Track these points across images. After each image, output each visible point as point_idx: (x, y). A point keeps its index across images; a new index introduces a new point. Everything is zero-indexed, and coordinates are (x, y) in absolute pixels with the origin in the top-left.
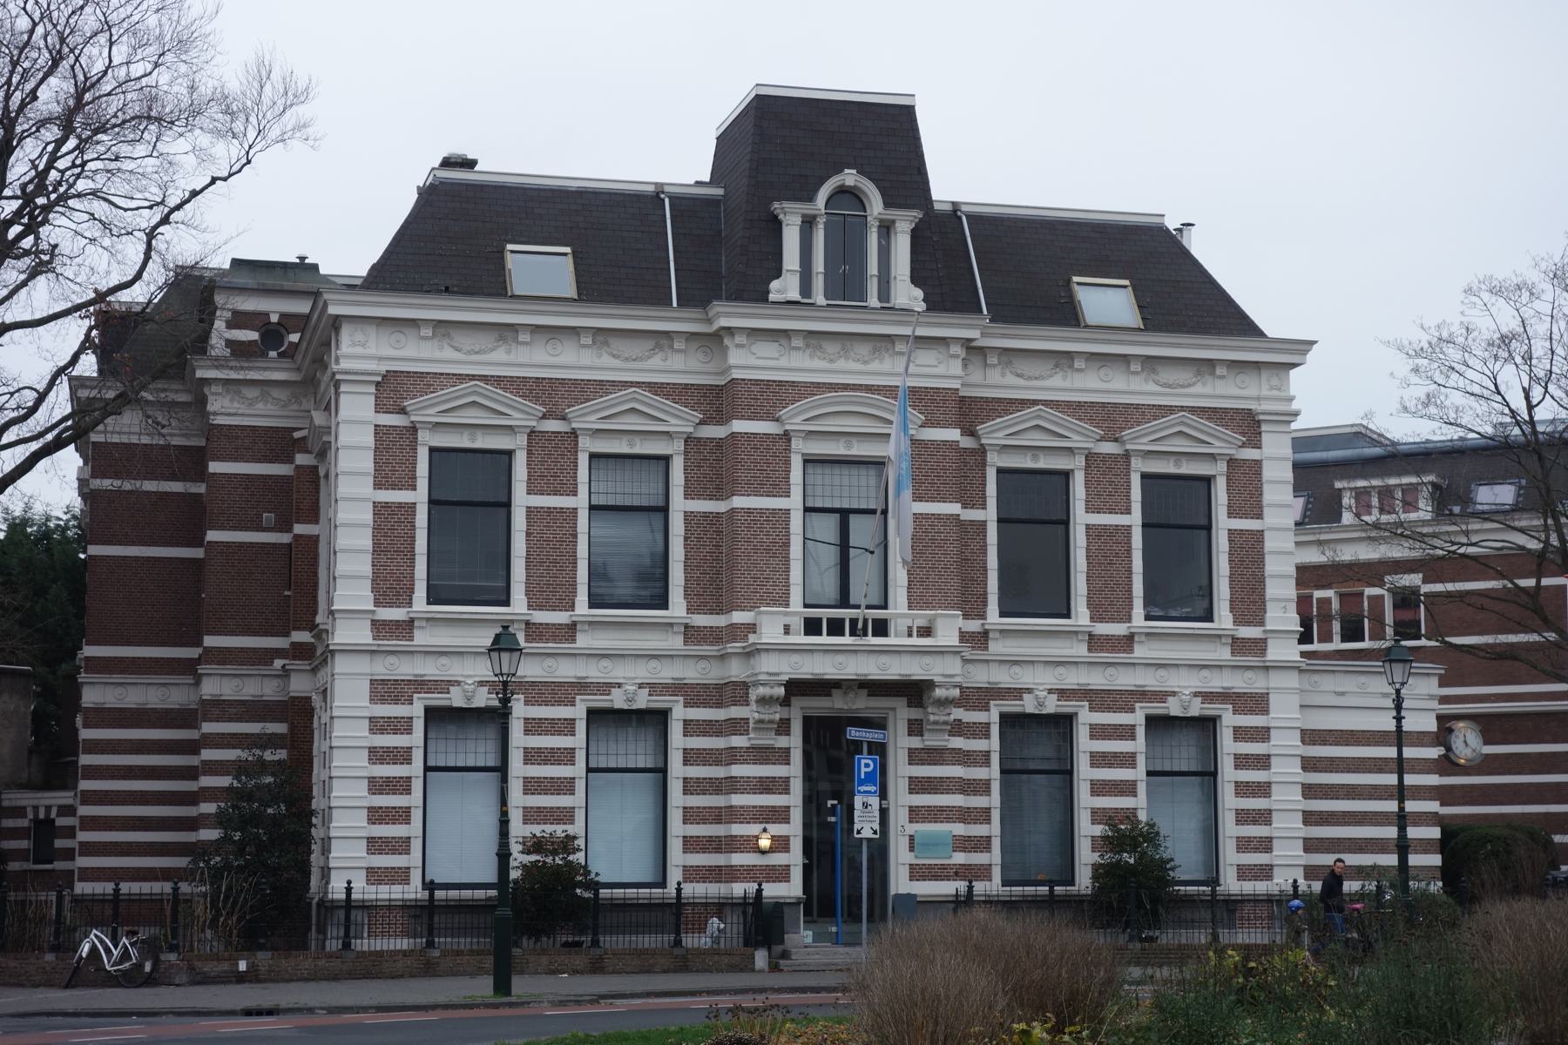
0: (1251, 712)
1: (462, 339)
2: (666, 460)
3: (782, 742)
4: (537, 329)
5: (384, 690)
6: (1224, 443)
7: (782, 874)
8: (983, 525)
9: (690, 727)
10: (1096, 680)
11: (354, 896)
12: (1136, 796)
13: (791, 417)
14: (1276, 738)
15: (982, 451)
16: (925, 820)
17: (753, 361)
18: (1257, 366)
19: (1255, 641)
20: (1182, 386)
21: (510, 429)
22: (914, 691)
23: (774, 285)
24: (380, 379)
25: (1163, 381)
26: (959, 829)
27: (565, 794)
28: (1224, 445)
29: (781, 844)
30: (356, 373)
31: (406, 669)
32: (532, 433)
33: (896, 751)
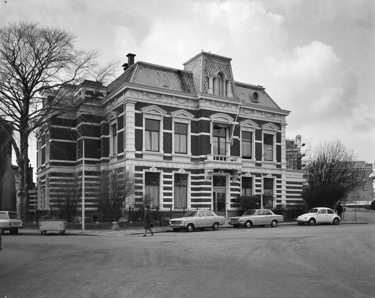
1: (151, 96)
6: (276, 129)
10: (165, 165)
11: (172, 210)
21: (188, 119)
24: (136, 103)
31: (141, 164)
32: (256, 130)
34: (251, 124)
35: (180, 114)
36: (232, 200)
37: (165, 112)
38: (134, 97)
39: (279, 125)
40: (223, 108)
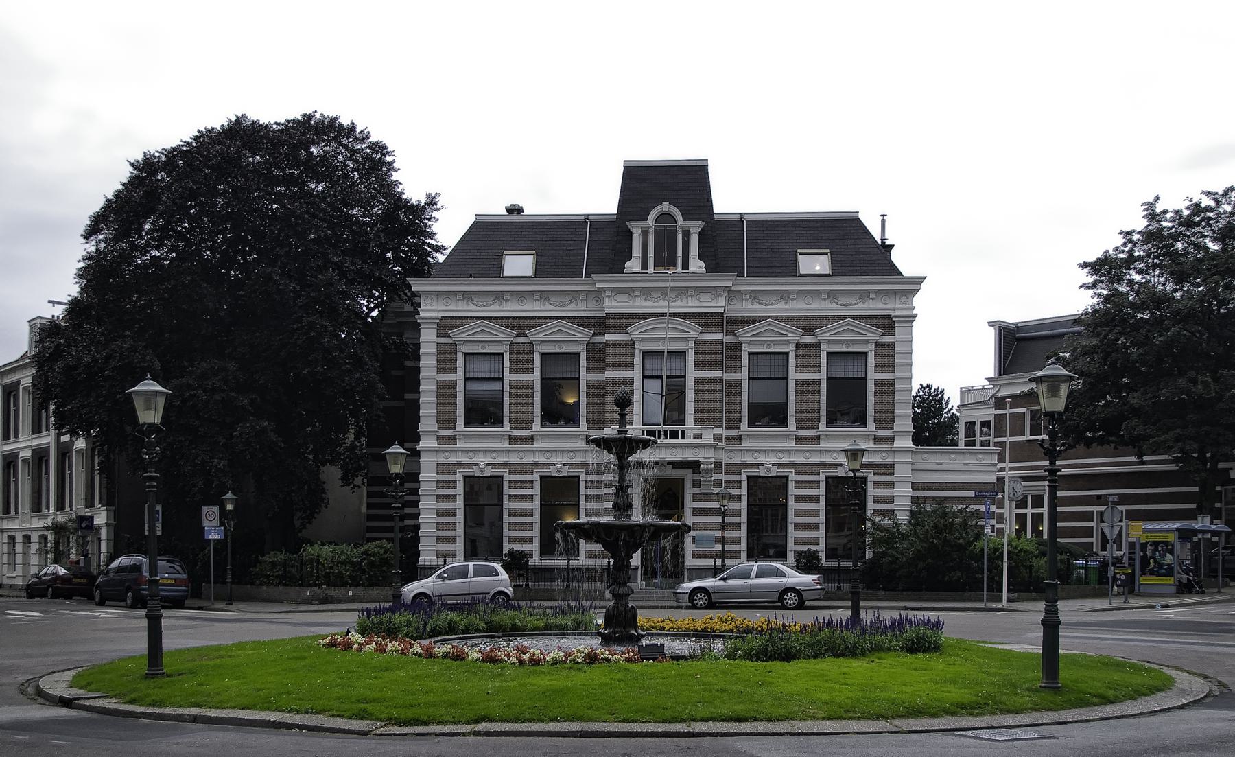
2: (865, 354)
4: (512, 293)
5: (444, 468)
6: (873, 334)
13: (632, 332)
14: (898, 489)
17: (615, 304)
18: (895, 292)
20: (851, 305)
22: (694, 466)
23: (627, 264)
24: (438, 321)
25: (840, 302)
28: (582, 336)
31: (453, 458)
32: (877, 344)
34: (782, 332)
38: (433, 308)
39: (888, 324)
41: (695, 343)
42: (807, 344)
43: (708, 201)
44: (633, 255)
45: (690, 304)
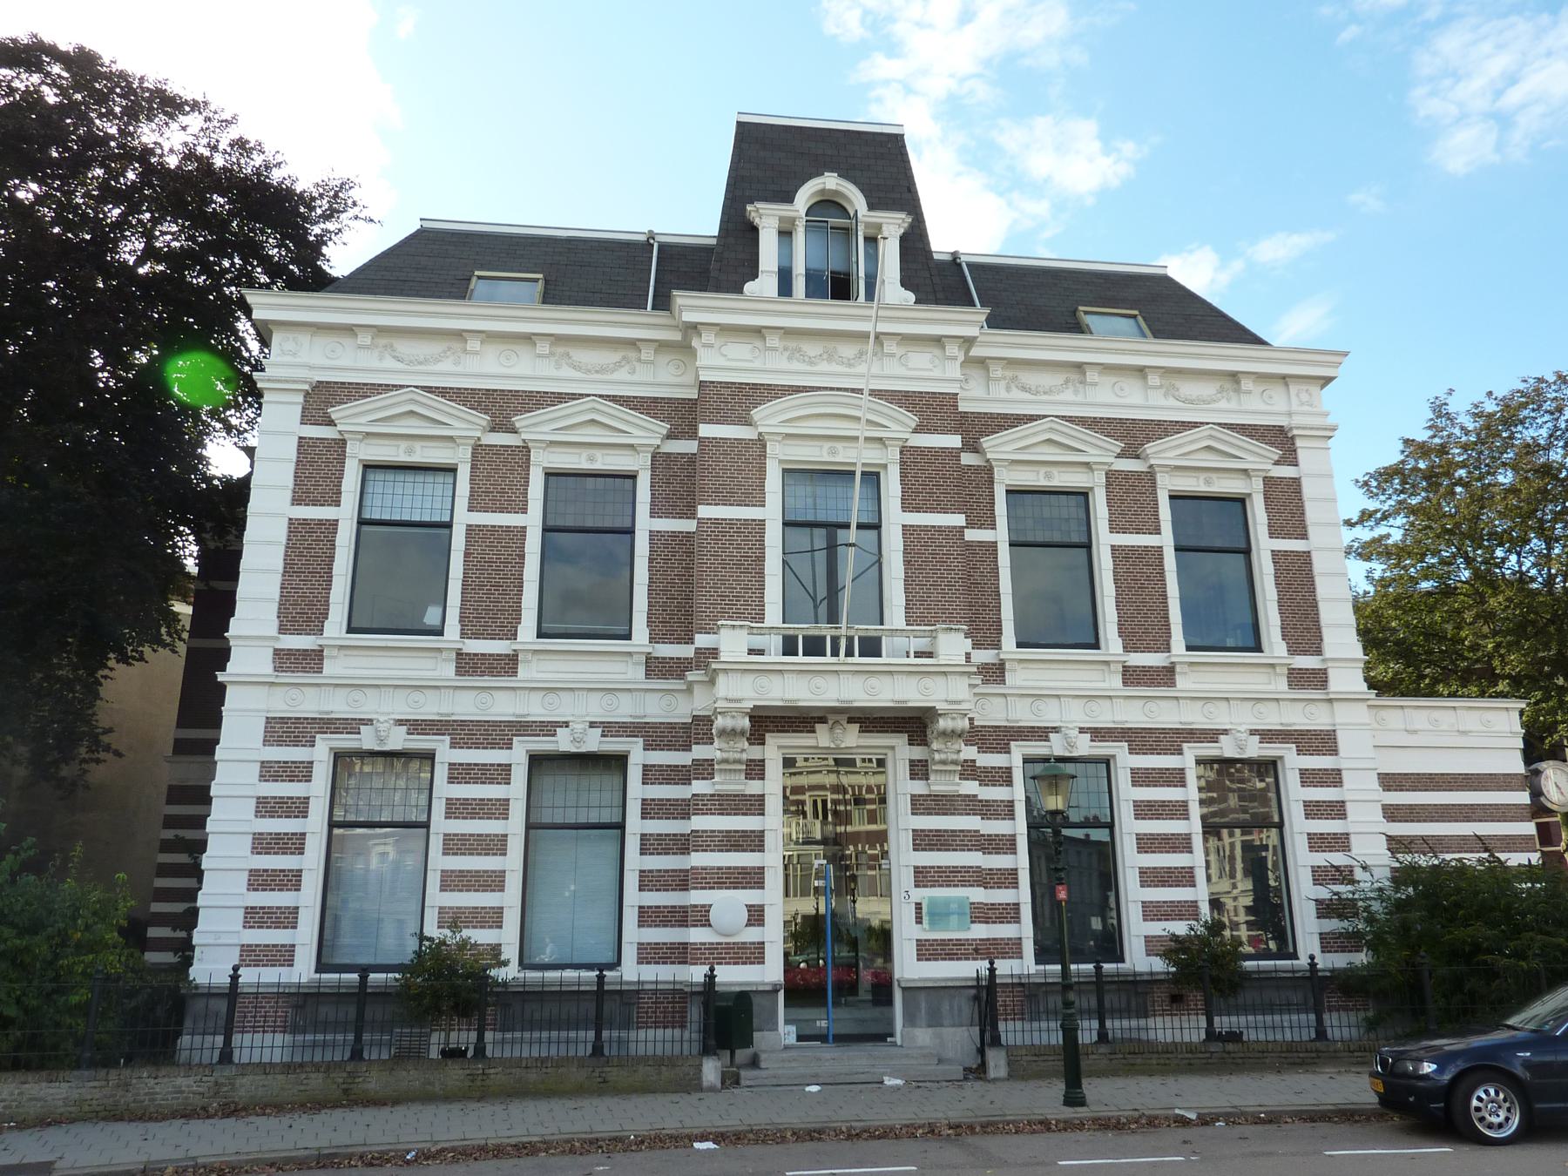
0: (1318, 752)
3: (754, 787)
5: (283, 730)
6: (1261, 459)
7: (755, 953)
8: (993, 546)
9: (651, 774)
10: (468, 705)
12: (1191, 852)
15: (1150, 476)
16: (935, 884)
17: (721, 362)
19: (1314, 672)
24: (306, 387)
26: (978, 895)
27: (495, 854)
29: (756, 916)
30: (279, 381)
33: (896, 798)
35: (1198, 450)
36: (1326, 909)
37: (1112, 448)
38: (298, 360)
40: (850, 365)
41: (901, 452)
42: (1127, 475)
43: (909, 191)
44: (761, 268)
45: (887, 372)
